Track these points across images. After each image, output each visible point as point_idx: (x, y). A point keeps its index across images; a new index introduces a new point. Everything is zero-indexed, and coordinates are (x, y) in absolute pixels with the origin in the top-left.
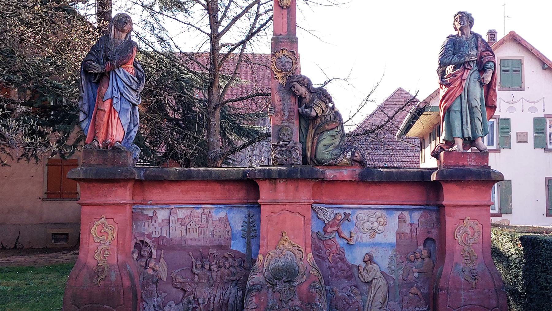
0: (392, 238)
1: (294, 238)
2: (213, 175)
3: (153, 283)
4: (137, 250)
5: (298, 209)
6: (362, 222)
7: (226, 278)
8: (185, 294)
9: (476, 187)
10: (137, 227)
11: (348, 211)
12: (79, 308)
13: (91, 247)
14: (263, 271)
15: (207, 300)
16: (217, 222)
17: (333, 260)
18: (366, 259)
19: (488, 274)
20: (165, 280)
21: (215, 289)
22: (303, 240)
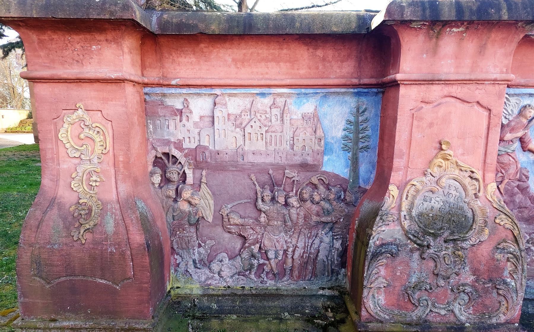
1: (463, 154)
2: (298, 24)
3: (190, 225)
4: (159, 171)
7: (315, 218)
8: (244, 243)
10: (155, 128)
12: (49, 283)
13: (64, 166)
14: (399, 219)
15: (281, 253)
16: (299, 123)
20: (210, 219)
21: (296, 236)
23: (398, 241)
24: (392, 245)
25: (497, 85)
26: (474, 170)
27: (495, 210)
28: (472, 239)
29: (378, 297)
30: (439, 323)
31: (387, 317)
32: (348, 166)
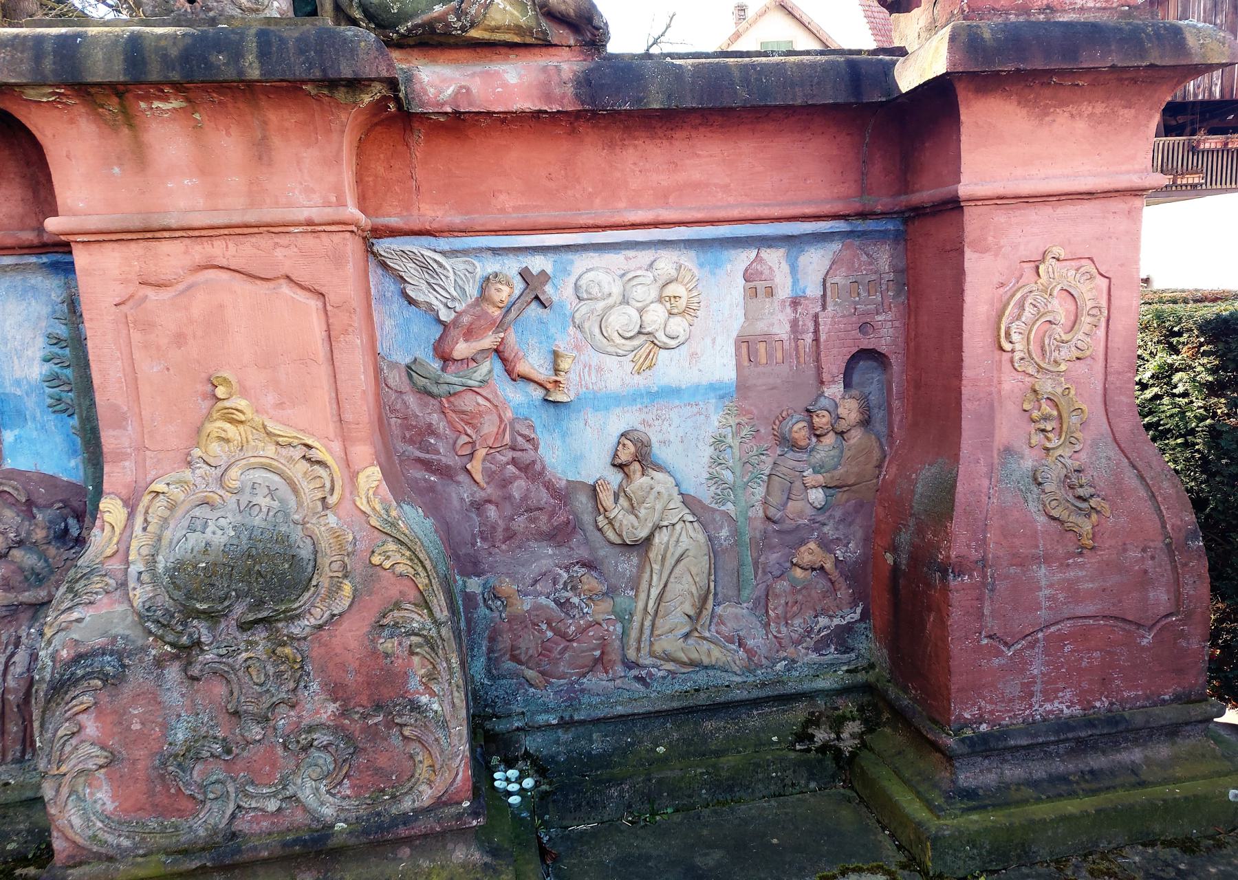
0: (720, 365)
1: (280, 405)
5: (283, 255)
6: (600, 305)
9: (1100, 108)
11: (537, 264)
14: (123, 585)
17: (490, 475)
18: (624, 457)
19: (1134, 483)
22: (329, 409)
23: (120, 641)
24: (104, 654)
25: (323, 234)
26: (310, 442)
27: (376, 532)
28: (313, 611)
29: (92, 794)
30: (269, 834)
31: (126, 843)
32: (75, 451)
